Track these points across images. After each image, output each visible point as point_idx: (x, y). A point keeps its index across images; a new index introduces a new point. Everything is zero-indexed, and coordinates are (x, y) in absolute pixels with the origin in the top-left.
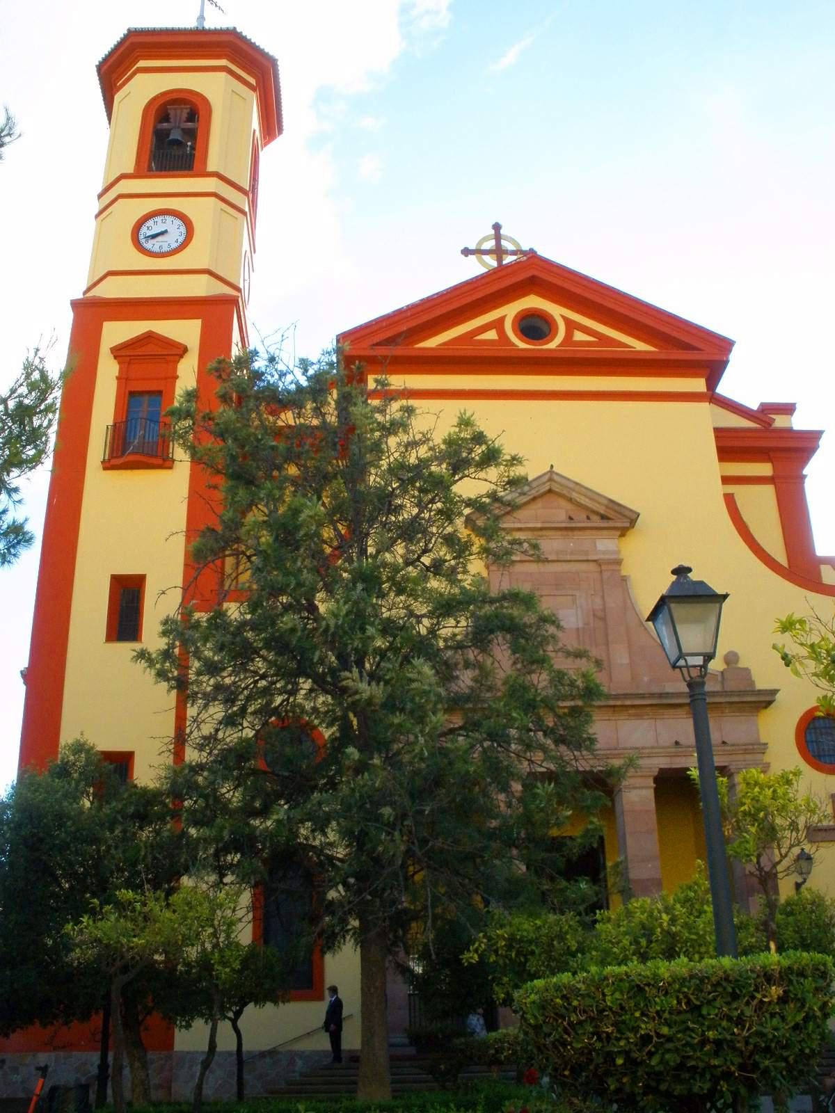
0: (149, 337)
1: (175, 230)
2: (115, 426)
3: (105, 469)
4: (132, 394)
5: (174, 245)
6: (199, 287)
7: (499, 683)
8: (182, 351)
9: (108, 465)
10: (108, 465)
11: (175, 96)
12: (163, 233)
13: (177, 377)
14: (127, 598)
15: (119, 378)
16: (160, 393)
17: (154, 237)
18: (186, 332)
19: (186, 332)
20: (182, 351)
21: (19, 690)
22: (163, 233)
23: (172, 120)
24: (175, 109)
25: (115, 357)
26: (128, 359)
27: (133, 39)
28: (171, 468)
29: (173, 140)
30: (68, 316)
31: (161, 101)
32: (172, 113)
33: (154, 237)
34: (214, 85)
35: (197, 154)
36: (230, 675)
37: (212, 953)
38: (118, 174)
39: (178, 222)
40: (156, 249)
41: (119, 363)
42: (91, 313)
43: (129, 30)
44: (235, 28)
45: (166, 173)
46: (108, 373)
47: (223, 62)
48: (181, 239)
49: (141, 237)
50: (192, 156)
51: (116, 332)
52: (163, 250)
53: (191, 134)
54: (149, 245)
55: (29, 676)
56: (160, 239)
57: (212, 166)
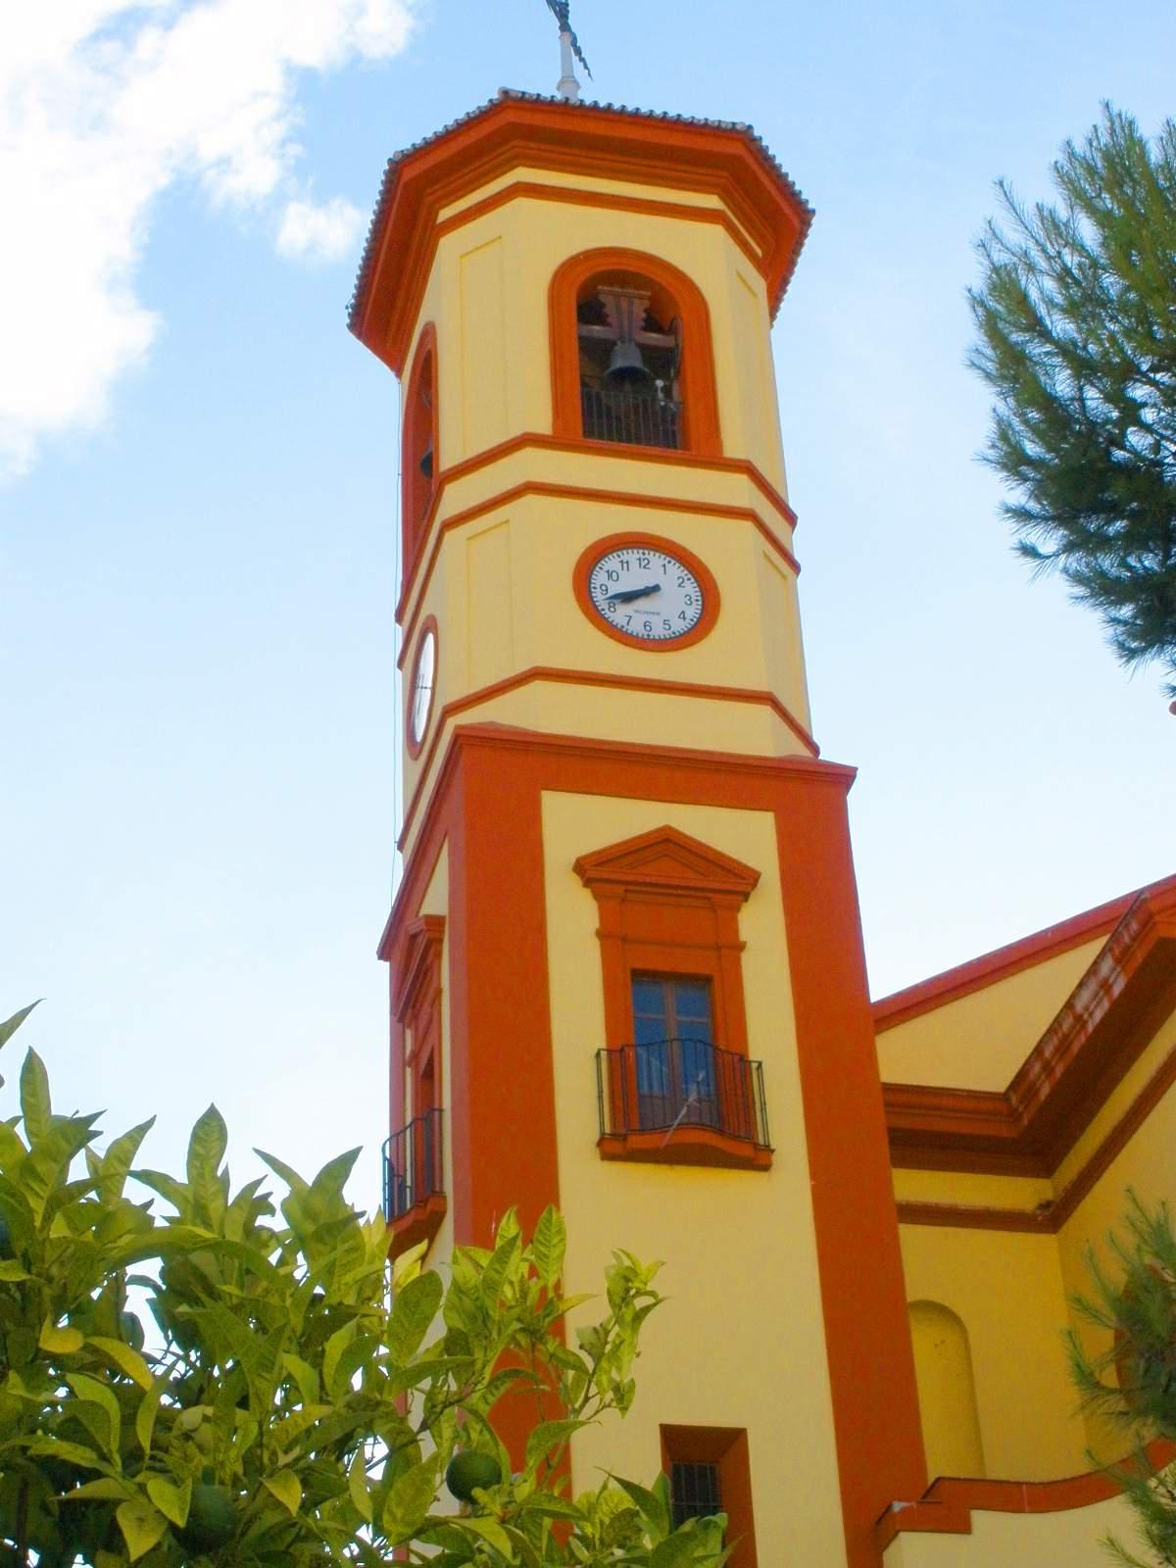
0: (666, 841)
3: (607, 1156)
4: (638, 975)
6: (750, 734)
8: (740, 881)
11: (632, 266)
12: (650, 591)
15: (603, 935)
16: (704, 981)
17: (628, 597)
18: (745, 835)
19: (745, 835)
20: (740, 881)
22: (650, 591)
24: (617, 296)
26: (620, 889)
27: (510, 116)
28: (765, 1167)
32: (608, 301)
33: (628, 597)
34: (702, 251)
37: (1128, 204)
38: (515, 432)
40: (636, 628)
41: (597, 896)
43: (505, 93)
44: (750, 127)
45: (615, 445)
46: (572, 922)
48: (679, 626)
49: (599, 596)
51: (577, 824)
54: (619, 615)
56: (641, 604)
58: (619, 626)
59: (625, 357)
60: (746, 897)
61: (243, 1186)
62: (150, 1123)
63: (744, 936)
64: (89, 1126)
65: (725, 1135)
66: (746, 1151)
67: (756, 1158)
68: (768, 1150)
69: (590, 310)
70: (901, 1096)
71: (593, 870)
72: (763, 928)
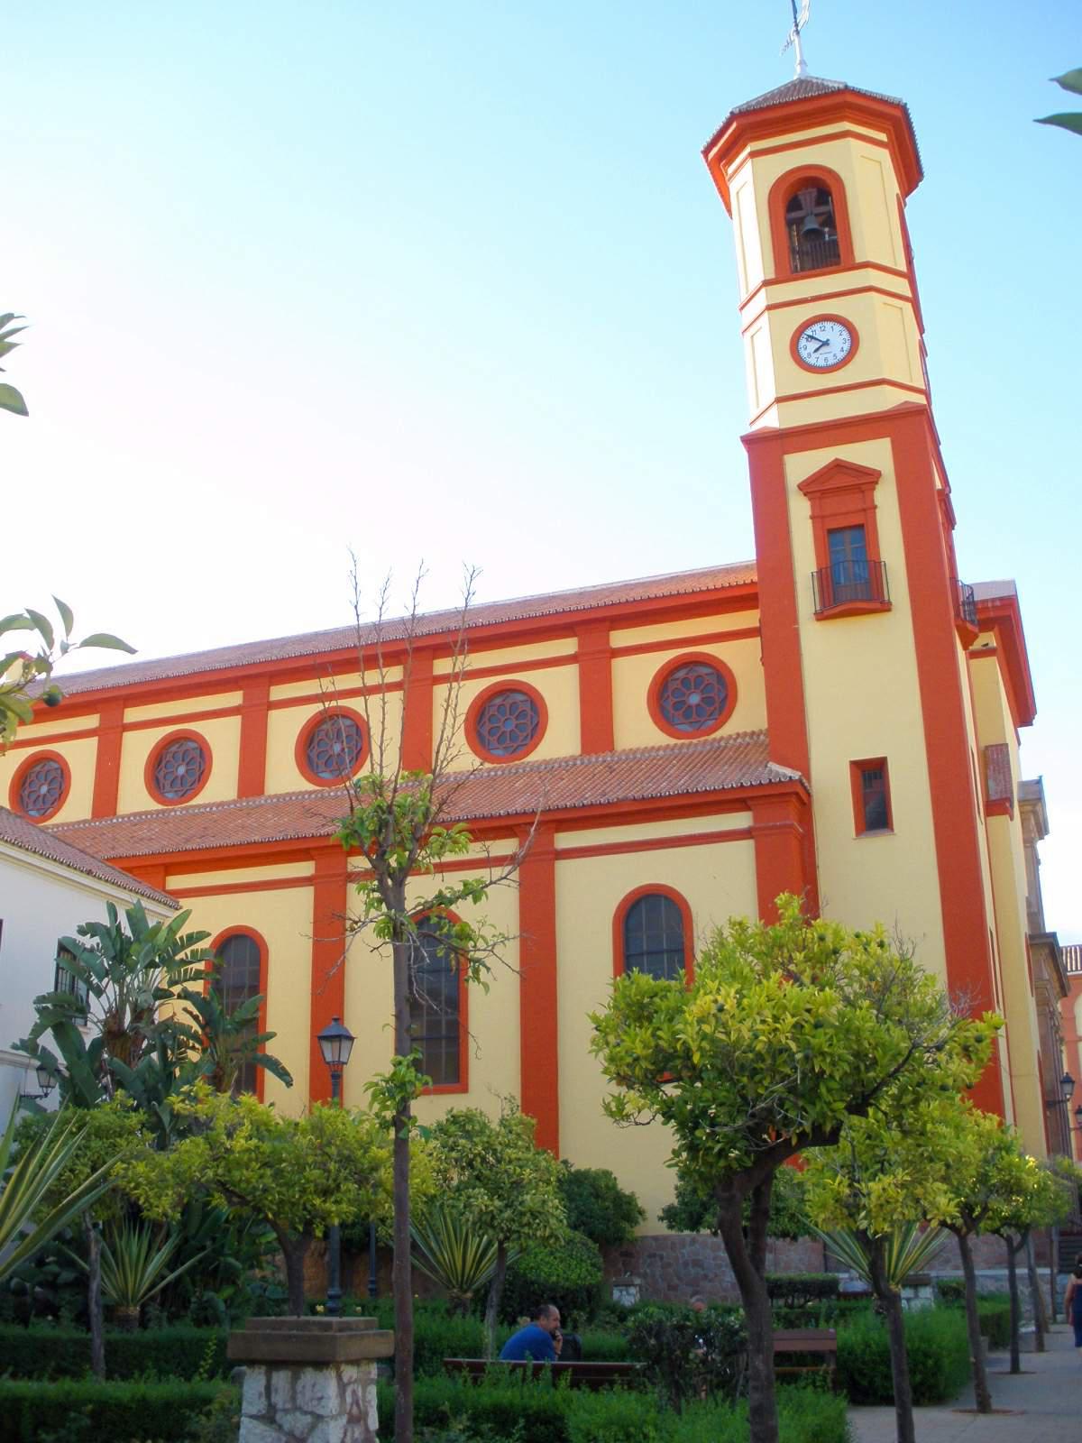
0: (839, 466)
1: (837, 339)
2: (820, 572)
3: (818, 620)
4: (830, 532)
5: (841, 356)
7: (498, 1129)
9: (821, 616)
10: (821, 616)
13: (875, 507)
14: (871, 777)
16: (861, 526)
18: (875, 454)
19: (875, 454)
20: (869, 478)
21: (1040, 857)
23: (804, 206)
25: (805, 495)
26: (819, 494)
28: (889, 610)
29: (810, 228)
30: (742, 456)
31: (793, 179)
35: (839, 236)
36: (889, 1106)
39: (838, 328)
41: (810, 500)
42: (766, 450)
45: (814, 272)
46: (800, 511)
47: (846, 126)
48: (847, 347)
50: (835, 243)
51: (801, 466)
52: (819, 325)
53: (829, 221)
55: (1038, 862)
57: (859, 258)
58: (148, 1317)
59: (811, 224)
60: (877, 483)
61: (20, 390)
62: (56, 600)
63: (876, 503)
64: (269, 1069)
65: (871, 600)
66: (878, 605)
67: (885, 607)
68: (889, 603)
69: (793, 204)
70: (756, 607)
71: (807, 488)
72: (886, 500)
